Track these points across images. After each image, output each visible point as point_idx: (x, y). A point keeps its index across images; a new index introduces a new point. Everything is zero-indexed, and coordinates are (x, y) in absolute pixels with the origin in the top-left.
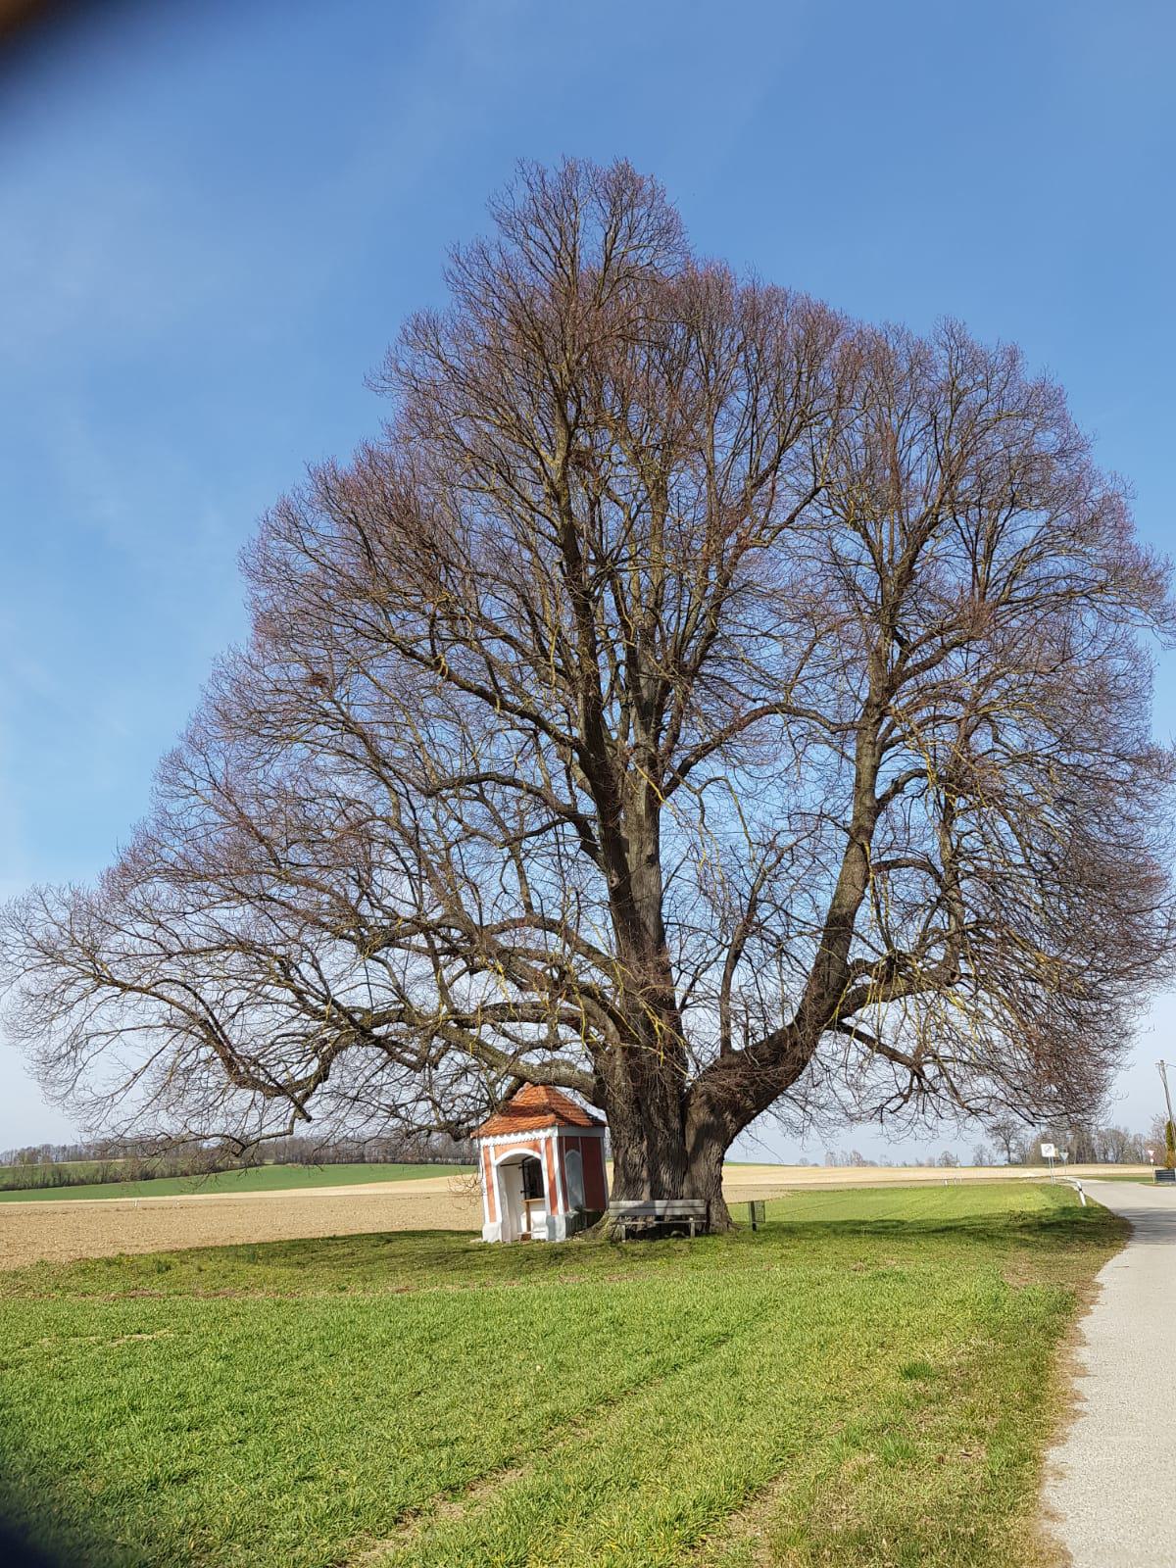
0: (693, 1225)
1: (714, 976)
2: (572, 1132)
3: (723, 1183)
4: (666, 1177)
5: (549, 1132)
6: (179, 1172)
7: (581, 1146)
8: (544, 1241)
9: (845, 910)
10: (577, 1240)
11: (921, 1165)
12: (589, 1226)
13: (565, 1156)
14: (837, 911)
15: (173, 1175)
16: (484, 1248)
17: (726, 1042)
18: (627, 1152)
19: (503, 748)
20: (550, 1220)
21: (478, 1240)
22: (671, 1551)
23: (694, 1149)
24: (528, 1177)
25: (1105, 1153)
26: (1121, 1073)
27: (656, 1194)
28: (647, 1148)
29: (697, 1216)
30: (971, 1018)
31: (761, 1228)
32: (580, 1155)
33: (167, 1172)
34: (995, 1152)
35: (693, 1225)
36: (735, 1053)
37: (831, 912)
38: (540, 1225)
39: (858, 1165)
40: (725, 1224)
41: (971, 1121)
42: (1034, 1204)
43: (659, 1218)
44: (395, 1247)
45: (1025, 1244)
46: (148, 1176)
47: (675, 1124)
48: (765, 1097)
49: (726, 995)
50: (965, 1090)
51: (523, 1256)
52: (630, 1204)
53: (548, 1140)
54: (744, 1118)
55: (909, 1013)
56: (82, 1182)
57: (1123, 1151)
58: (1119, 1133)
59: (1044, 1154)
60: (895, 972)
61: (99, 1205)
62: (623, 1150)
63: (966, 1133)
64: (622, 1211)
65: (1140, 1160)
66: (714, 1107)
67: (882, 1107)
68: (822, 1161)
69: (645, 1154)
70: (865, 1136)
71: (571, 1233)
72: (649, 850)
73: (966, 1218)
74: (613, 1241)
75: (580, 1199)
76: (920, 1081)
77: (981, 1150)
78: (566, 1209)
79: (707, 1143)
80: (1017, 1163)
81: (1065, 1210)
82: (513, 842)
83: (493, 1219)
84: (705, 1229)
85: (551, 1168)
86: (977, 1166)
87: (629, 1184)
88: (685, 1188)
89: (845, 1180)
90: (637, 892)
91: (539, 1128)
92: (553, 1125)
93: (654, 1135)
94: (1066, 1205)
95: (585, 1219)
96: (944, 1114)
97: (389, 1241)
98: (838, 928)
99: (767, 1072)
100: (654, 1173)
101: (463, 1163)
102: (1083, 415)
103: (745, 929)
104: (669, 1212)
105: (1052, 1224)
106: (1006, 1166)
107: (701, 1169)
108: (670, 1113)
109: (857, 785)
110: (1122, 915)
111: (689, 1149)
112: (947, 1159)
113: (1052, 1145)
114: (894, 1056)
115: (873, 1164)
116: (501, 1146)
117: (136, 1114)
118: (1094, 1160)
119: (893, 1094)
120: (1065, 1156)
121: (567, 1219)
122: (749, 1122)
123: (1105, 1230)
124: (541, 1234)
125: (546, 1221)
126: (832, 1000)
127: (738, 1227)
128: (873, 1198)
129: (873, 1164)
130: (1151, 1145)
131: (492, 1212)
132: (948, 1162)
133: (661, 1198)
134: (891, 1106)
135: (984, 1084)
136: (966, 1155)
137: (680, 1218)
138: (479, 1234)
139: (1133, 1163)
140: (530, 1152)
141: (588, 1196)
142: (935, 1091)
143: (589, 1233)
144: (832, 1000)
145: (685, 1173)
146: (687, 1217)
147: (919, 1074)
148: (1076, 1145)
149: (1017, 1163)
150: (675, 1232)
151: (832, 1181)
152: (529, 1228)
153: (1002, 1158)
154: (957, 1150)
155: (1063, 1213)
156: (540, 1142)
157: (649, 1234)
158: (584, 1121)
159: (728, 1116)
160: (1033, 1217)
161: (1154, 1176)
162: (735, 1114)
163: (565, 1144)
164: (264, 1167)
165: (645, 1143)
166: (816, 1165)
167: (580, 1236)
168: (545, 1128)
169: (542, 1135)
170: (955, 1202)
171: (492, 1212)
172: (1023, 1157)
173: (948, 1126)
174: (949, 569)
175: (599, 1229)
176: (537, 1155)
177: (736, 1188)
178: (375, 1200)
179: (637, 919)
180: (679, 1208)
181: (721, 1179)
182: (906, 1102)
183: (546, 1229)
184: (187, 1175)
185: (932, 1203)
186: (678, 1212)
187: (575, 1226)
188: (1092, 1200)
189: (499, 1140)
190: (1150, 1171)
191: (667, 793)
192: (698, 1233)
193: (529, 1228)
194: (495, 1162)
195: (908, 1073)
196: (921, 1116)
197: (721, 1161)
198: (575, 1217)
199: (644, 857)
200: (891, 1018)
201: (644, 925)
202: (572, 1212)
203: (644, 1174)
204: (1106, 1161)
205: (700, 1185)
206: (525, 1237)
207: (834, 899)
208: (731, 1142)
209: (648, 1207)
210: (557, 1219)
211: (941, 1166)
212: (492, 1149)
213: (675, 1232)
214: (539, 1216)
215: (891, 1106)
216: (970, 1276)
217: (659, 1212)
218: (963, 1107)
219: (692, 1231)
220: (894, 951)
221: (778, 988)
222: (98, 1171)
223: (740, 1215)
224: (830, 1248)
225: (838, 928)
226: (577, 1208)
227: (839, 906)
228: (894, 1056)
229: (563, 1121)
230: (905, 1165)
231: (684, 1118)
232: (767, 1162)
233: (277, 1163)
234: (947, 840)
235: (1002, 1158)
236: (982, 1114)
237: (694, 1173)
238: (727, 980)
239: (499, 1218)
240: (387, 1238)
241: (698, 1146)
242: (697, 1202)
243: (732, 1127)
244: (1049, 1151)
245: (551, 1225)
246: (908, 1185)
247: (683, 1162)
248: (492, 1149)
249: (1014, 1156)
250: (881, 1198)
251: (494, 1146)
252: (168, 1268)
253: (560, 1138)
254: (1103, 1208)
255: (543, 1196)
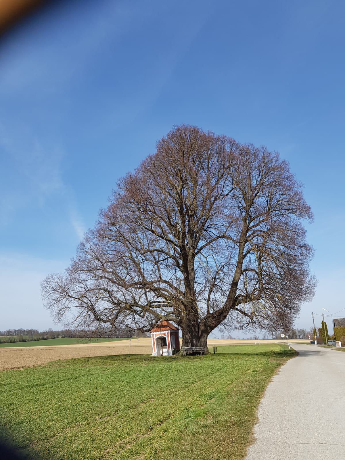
0: (201, 353)
1: (206, 295)
2: (173, 331)
3: (207, 344)
4: (194, 342)
5: (167, 332)
6: (33, 340)
7: (175, 335)
8: (167, 356)
9: (236, 281)
10: (174, 356)
11: (248, 339)
12: (177, 353)
13: (171, 337)
14: (234, 281)
15: (31, 341)
16: (154, 357)
17: (208, 311)
18: (186, 336)
19: (162, 244)
20: (168, 351)
21: (151, 356)
22: (250, 367)
23: (201, 335)
24: (162, 342)
25: (300, 336)
26: (297, 319)
27: (192, 346)
28: (191, 335)
29: (202, 350)
30: (265, 308)
31: (215, 353)
32: (174, 337)
33: (30, 340)
34: (269, 335)
35: (201, 353)
36: (210, 314)
37: (233, 281)
38: (165, 352)
39: (230, 339)
40: (208, 352)
41: (263, 330)
42: (278, 349)
43: (193, 351)
44: (132, 357)
45: (274, 357)
46: (24, 341)
47: (197, 330)
48: (218, 323)
49: (209, 300)
50: (262, 323)
51: (161, 358)
52: (187, 348)
53: (168, 333)
54: (212, 328)
55: (251, 307)
56: (5, 342)
57: (303, 335)
58: (304, 331)
59: (281, 337)
60: (248, 297)
61: (12, 349)
62: (185, 336)
63: (262, 332)
64: (185, 349)
65: (308, 338)
66: (205, 325)
67: (243, 326)
68: (220, 338)
69: (190, 337)
70: (235, 333)
71: (173, 354)
72: (192, 267)
73: (261, 352)
74: (183, 356)
75: (174, 346)
76: (252, 320)
77: (265, 335)
78: (172, 349)
79: (204, 334)
80: (275, 339)
81: (285, 351)
82: (156, 263)
83: (155, 351)
84: (203, 353)
85: (168, 339)
86: (264, 339)
87: (186, 343)
88: (199, 344)
89: (227, 343)
90: (190, 277)
91: (165, 331)
92: (169, 330)
93: (192, 331)
94: (286, 349)
95: (176, 350)
96: (257, 328)
97: (129, 356)
98: (234, 284)
99: (218, 317)
100: (192, 341)
101: (117, 338)
102: (293, 170)
103: (213, 286)
104: (196, 350)
105: (281, 353)
106: (272, 340)
107: (202, 340)
108: (196, 327)
109: (239, 252)
110: (297, 286)
111: (200, 335)
112: (255, 337)
113: (284, 334)
114: (246, 315)
115: (234, 339)
116: (156, 334)
117: (76, 326)
118: (296, 338)
119: (245, 323)
120: (287, 337)
121: (172, 351)
122: (213, 329)
123: (293, 354)
124: (165, 354)
125: (166, 352)
126: (233, 301)
127: (210, 353)
128: (236, 348)
129: (234, 339)
130: (309, 333)
131: (155, 349)
132: (256, 338)
133: (193, 346)
134: (245, 326)
135: (266, 322)
136: (261, 336)
137: (198, 351)
138: (152, 355)
139: (307, 339)
140: (163, 336)
141: (176, 346)
142: (255, 323)
143: (177, 354)
144: (233, 301)
145: (199, 341)
146: (199, 351)
147: (252, 319)
148: (291, 334)
149: (275, 339)
150: (197, 354)
151: (221, 343)
152: (162, 353)
153: (271, 337)
154: (257, 335)
155: (285, 351)
156: (166, 334)
157: (190, 354)
158: (175, 329)
159: (208, 328)
160: (276, 352)
161: (310, 343)
162: (210, 328)
163: (172, 334)
164: (58, 339)
165: (190, 334)
166: (218, 339)
167: (175, 355)
168: (167, 330)
169: (166, 332)
170: (258, 349)
171: (155, 349)
172: (277, 337)
173: (258, 330)
174: (261, 201)
175: (179, 353)
176: (165, 337)
177: (211, 345)
178: (103, 348)
179: (189, 282)
180: (198, 349)
181: (207, 342)
182: (248, 325)
183: (167, 353)
184: (35, 341)
185: (252, 349)
186: (198, 350)
187: (174, 353)
188: (292, 348)
189: (156, 333)
190: (309, 341)
191: (197, 254)
192: (202, 354)
193: (162, 353)
194: (155, 338)
195: (249, 318)
196: (252, 328)
197: (207, 338)
198: (174, 351)
199: (191, 269)
200: (247, 307)
201: (191, 285)
202: (173, 350)
203: (190, 341)
204: (300, 339)
205: (202, 343)
206: (162, 355)
207: (233, 279)
208: (209, 334)
209: (191, 349)
210: (170, 351)
211: (254, 339)
212: (154, 335)
213: (197, 354)
214: (165, 350)
215: (245, 326)
216: (263, 360)
217: (193, 349)
218: (261, 326)
219: (201, 354)
220: (248, 293)
221: (220, 299)
222: (9, 339)
223: (211, 351)
224: (233, 357)
225: (234, 284)
226: (174, 349)
227: (235, 280)
228: (246, 315)
229: (171, 329)
230: (244, 339)
231: (199, 328)
232: (215, 339)
233: (63, 337)
234: (259, 267)
235: (271, 337)
236: (266, 328)
237: (201, 341)
238: (209, 296)
239: (156, 351)
240: (130, 355)
241: (202, 335)
242: (202, 347)
243: (209, 331)
244: (283, 336)
245: (168, 352)
246: (245, 344)
247: (199, 338)
248: (154, 335)
249: (274, 337)
250: (238, 348)
251: (155, 334)
252: (89, 361)
253: (170, 333)
254: (295, 350)
255: (166, 346)
